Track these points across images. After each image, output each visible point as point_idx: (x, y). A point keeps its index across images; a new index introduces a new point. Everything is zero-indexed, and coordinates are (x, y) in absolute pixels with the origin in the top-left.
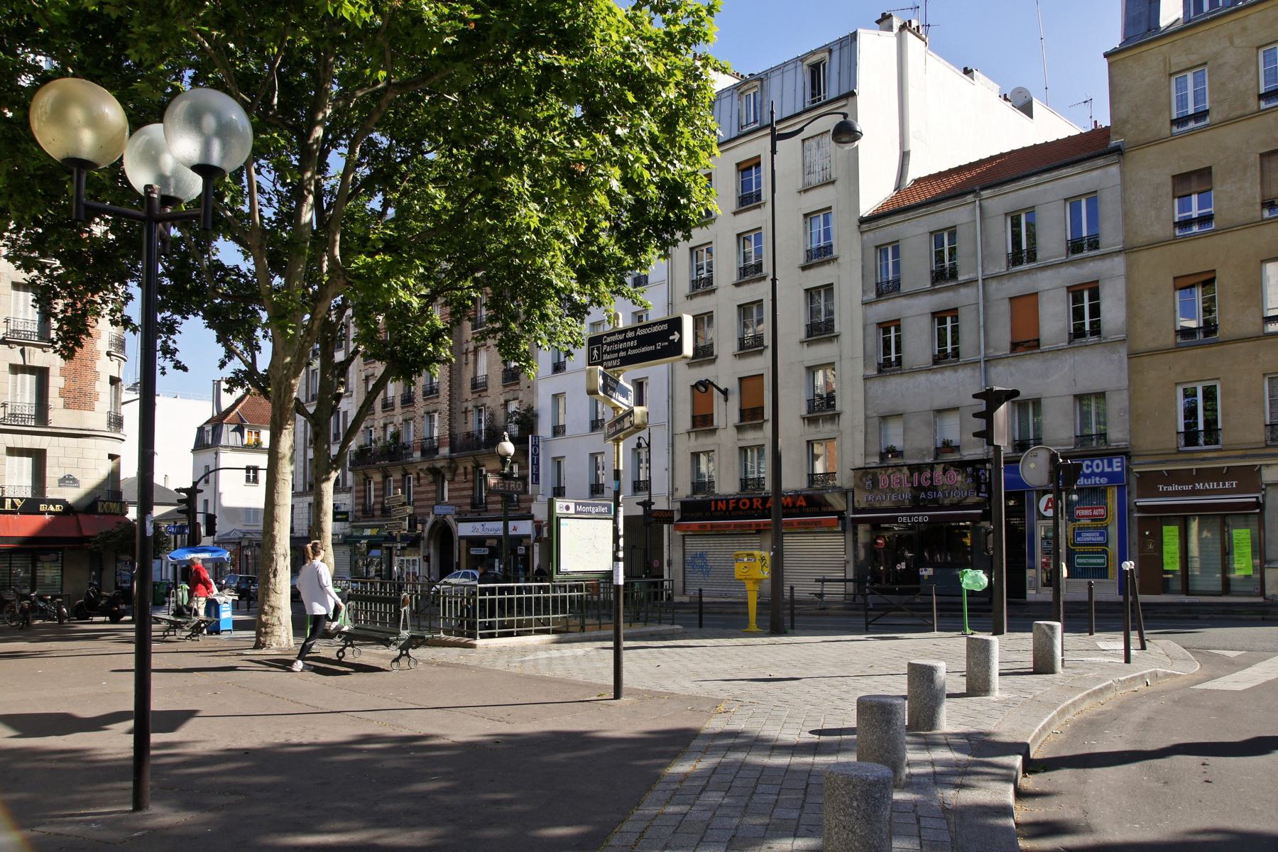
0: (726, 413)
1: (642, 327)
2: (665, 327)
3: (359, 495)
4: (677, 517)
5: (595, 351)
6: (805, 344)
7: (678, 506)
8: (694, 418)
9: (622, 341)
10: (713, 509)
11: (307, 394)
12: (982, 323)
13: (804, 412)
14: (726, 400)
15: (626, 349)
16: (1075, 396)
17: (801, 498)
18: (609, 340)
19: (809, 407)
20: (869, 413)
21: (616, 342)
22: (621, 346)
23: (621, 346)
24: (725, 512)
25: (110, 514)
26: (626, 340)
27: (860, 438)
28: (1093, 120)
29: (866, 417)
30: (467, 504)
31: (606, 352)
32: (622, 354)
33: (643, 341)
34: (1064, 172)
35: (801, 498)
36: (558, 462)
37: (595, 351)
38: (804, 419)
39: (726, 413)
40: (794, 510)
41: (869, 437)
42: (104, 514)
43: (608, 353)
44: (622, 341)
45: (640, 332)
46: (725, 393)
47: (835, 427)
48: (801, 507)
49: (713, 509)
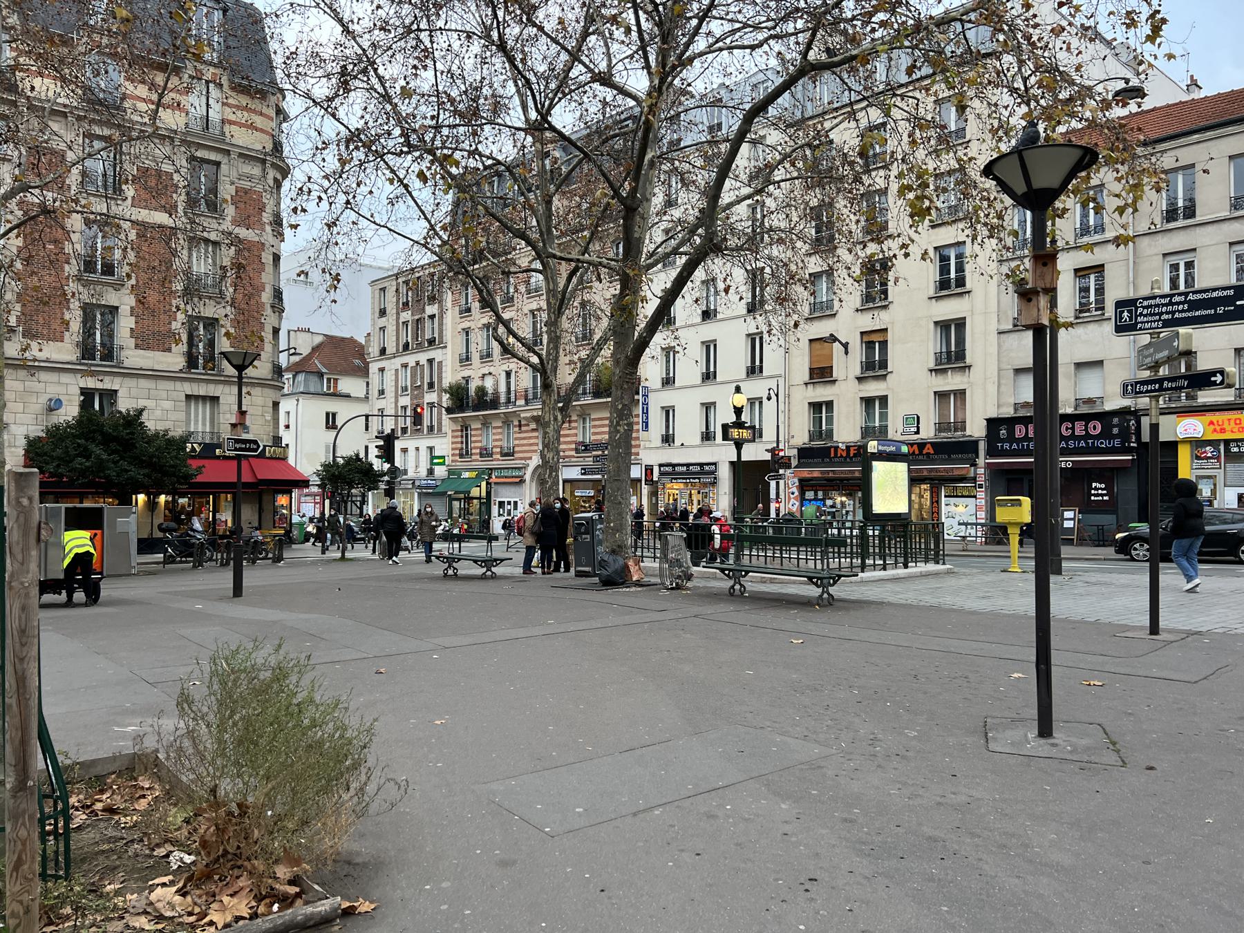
0: (847, 366)
1: (1194, 293)
2: (1232, 292)
3: (637, 443)
4: (794, 462)
5: (1126, 314)
6: (934, 300)
7: (795, 452)
8: (811, 370)
9: (1166, 305)
10: (832, 455)
11: (398, 345)
12: (1131, 279)
13: (932, 365)
14: (847, 353)
15: (1173, 313)
16: (1235, 349)
17: (929, 446)
18: (1145, 303)
19: (936, 359)
20: (1004, 366)
21: (1157, 306)
22: (1164, 309)
23: (1164, 309)
24: (845, 458)
25: (276, 458)
26: (1171, 304)
27: (992, 389)
28: (1190, 74)
29: (999, 370)
30: (571, 450)
31: (1141, 314)
32: (1165, 317)
33: (1194, 305)
34: (1230, 129)
35: (929, 446)
36: (668, 411)
37: (1126, 314)
38: (931, 371)
39: (847, 366)
40: (921, 457)
41: (1003, 388)
42: (271, 458)
43: (1145, 316)
44: (1166, 305)
45: (1191, 297)
46: (846, 346)
47: (965, 379)
48: (928, 454)
49: (832, 455)
